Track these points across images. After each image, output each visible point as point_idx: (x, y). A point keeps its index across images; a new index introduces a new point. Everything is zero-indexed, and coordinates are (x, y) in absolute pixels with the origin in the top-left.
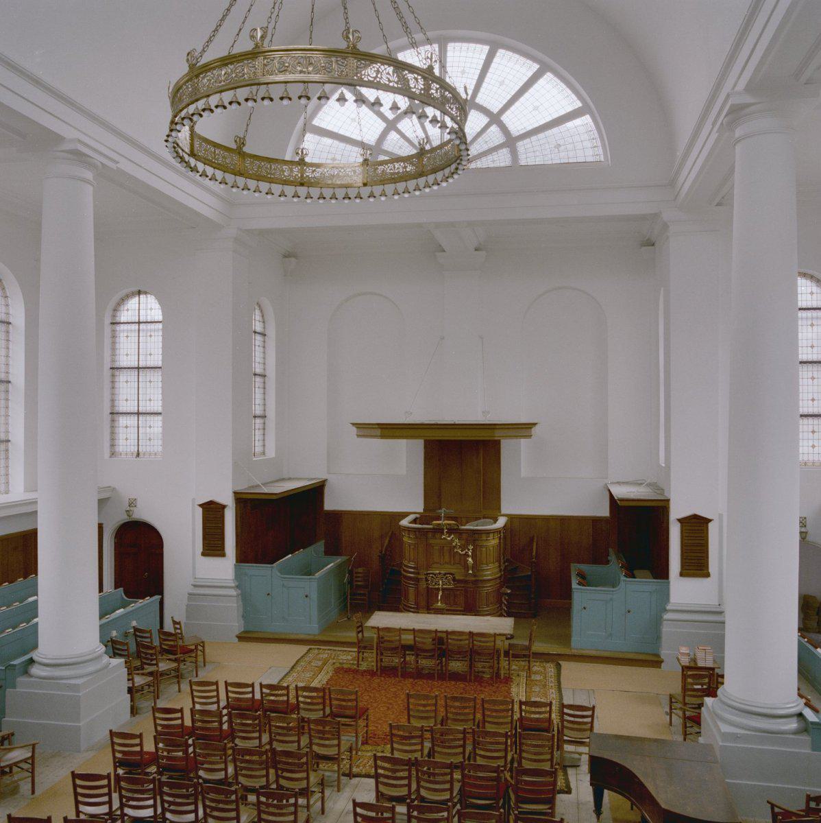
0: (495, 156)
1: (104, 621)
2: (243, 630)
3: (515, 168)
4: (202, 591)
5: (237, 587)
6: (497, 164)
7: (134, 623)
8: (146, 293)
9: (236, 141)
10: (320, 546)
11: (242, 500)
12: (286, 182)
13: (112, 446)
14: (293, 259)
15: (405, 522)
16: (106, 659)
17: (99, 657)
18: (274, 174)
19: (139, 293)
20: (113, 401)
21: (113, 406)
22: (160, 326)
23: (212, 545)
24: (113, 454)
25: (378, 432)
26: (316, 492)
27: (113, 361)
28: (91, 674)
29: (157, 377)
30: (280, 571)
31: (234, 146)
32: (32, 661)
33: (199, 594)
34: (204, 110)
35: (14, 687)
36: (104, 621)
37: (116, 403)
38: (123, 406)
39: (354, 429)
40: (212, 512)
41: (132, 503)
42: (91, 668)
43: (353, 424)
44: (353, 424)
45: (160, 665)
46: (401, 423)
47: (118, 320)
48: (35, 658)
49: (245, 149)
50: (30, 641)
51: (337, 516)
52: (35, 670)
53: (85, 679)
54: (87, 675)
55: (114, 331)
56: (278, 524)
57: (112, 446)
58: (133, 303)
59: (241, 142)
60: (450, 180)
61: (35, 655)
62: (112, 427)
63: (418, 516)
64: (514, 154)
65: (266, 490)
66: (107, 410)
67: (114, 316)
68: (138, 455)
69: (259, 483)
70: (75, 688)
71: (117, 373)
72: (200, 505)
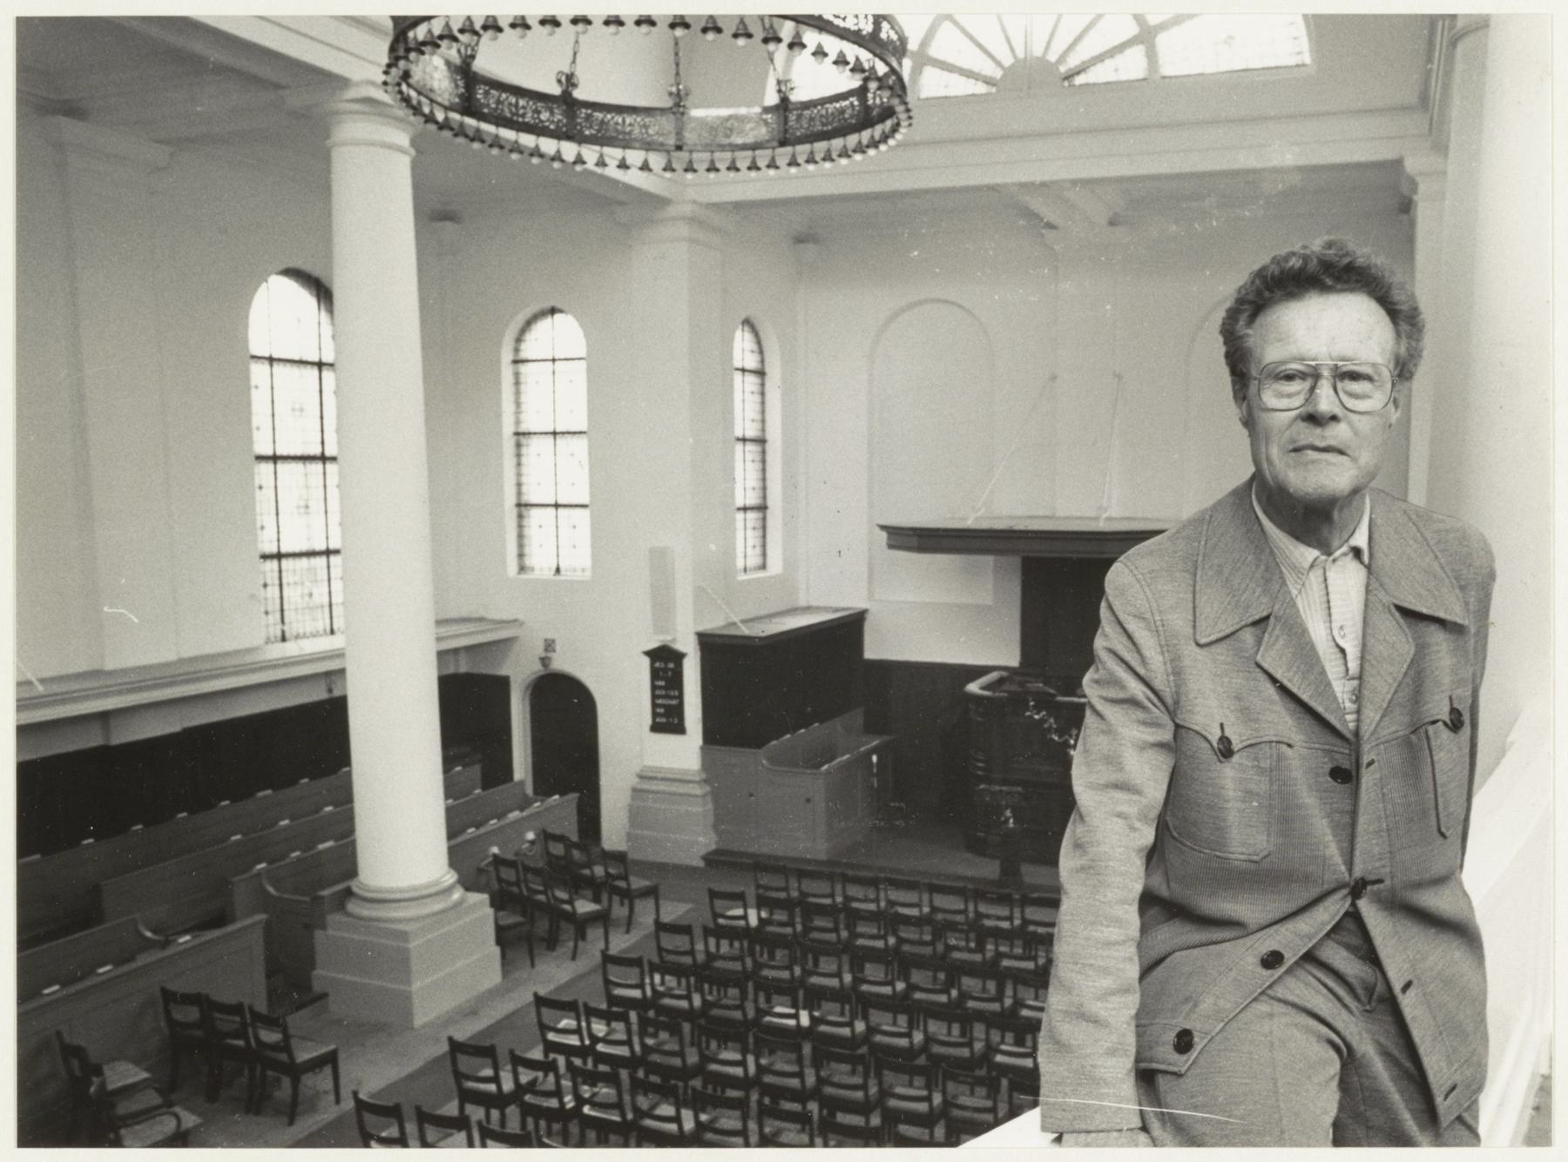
0: (1119, 60)
1: (454, 842)
2: (714, 847)
3: (1154, 85)
4: (653, 786)
5: (705, 781)
6: (1123, 76)
7: (495, 850)
8: (561, 311)
9: (559, 81)
10: (857, 717)
11: (708, 643)
12: (649, 146)
13: (521, 555)
14: (810, 246)
15: (973, 687)
16: (457, 894)
17: (449, 890)
18: (630, 133)
19: (553, 311)
20: (519, 485)
21: (519, 493)
22: (583, 364)
23: (668, 720)
24: (522, 569)
25: (914, 541)
26: (850, 628)
27: (518, 422)
28: (435, 914)
29: (580, 446)
30: (770, 759)
31: (556, 90)
32: (349, 893)
33: (648, 785)
34: (441, 37)
35: (324, 927)
36: (454, 842)
37: (524, 489)
38: (531, 496)
39: (884, 535)
40: (665, 662)
41: (549, 645)
42: (438, 906)
43: (883, 527)
44: (883, 527)
45: (632, 879)
46: (970, 523)
47: (523, 355)
48: (355, 889)
49: (578, 94)
50: (347, 864)
51: (886, 669)
52: (352, 906)
53: (418, 925)
54: (428, 916)
55: (517, 375)
56: (771, 684)
57: (521, 555)
58: (543, 327)
59: (569, 81)
60: (883, 147)
61: (354, 885)
62: (520, 526)
63: (1005, 674)
64: (1152, 56)
65: (745, 631)
66: (510, 500)
67: (517, 350)
68: (558, 570)
69: (736, 619)
70: (404, 936)
71: (523, 440)
72: (648, 653)
